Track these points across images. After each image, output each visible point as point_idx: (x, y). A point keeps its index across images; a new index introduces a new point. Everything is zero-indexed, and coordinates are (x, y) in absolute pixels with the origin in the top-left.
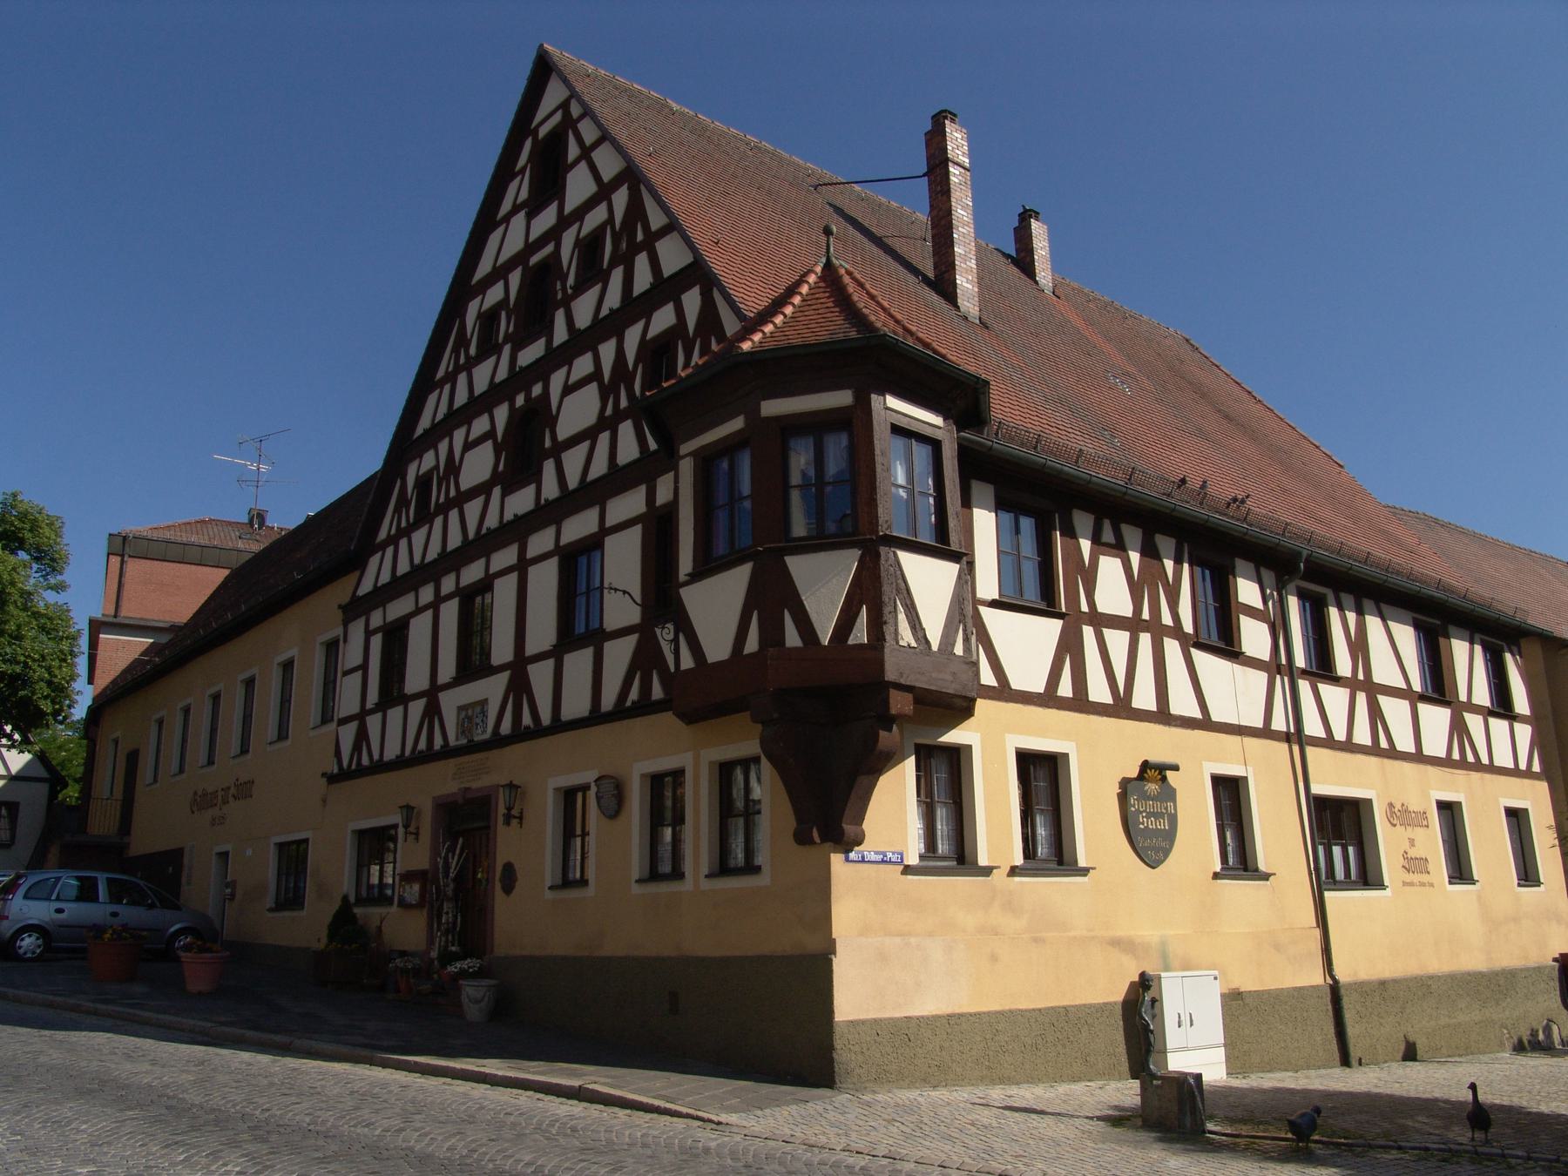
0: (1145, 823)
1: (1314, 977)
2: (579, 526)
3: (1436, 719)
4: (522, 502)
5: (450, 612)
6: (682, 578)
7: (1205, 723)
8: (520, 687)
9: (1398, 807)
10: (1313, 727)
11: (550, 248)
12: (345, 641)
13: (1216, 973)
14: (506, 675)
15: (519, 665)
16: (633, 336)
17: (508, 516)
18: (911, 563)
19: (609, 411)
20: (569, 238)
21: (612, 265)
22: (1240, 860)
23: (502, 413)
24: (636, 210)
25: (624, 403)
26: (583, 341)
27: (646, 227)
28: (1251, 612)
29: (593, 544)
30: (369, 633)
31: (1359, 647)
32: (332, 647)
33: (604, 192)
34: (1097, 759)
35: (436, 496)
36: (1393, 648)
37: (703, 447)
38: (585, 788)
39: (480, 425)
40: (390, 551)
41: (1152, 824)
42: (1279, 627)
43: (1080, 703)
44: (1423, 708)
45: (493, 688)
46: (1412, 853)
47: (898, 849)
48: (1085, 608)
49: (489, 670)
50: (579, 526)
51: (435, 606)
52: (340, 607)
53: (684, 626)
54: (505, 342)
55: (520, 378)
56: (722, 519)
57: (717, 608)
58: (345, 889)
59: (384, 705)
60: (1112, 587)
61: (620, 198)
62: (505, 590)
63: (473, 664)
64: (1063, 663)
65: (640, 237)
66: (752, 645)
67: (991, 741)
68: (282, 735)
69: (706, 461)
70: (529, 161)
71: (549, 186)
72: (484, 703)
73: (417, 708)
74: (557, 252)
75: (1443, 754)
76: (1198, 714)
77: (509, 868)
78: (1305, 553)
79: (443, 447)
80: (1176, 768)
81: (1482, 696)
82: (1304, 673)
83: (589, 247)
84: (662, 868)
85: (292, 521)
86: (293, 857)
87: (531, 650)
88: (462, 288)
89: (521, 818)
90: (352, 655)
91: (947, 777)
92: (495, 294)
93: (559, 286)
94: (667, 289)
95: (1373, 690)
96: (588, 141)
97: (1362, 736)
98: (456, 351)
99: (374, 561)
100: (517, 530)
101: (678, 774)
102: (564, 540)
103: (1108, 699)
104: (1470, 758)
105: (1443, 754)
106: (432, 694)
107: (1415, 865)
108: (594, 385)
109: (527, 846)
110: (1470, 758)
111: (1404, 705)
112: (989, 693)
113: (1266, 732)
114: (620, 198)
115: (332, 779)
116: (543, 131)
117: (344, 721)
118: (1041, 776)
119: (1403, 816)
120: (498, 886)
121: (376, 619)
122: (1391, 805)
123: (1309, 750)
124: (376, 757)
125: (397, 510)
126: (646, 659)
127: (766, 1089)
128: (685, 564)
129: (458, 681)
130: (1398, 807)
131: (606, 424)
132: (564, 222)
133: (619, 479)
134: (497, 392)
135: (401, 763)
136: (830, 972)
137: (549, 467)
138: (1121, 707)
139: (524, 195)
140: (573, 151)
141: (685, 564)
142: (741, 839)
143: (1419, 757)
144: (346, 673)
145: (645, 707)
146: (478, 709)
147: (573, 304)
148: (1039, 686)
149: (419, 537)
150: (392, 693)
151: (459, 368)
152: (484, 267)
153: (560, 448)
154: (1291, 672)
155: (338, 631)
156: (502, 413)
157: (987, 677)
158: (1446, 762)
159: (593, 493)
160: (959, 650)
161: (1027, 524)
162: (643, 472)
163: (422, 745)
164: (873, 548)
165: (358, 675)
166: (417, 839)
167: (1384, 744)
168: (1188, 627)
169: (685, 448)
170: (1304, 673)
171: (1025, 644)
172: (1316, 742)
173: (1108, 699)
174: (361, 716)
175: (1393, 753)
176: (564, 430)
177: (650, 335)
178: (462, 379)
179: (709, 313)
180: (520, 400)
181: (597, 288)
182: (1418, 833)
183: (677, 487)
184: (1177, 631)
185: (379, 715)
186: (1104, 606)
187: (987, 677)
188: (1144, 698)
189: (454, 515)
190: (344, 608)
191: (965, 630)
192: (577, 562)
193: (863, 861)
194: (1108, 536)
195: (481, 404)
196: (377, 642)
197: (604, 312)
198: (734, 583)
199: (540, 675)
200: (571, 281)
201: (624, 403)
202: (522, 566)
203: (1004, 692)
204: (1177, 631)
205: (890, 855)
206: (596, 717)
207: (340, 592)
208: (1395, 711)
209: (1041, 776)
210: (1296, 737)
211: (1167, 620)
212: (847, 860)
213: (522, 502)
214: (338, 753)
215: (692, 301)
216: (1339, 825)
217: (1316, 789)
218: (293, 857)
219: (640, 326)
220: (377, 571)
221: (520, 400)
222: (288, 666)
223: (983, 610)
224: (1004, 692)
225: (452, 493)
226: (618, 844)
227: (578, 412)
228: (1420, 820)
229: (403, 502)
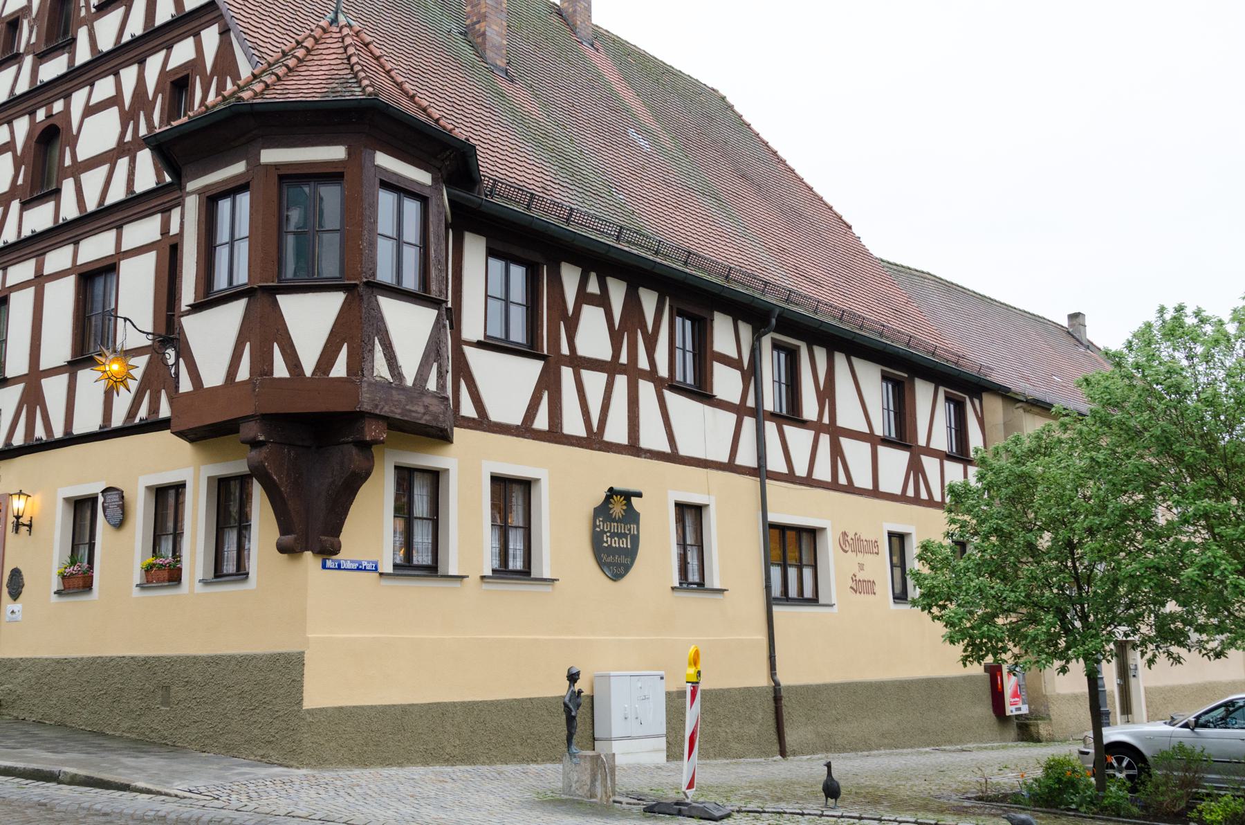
0: (608, 541)
1: (763, 681)
2: (96, 248)
3: (894, 462)
4: (40, 218)
6: (184, 308)
7: (673, 457)
8: (33, 399)
9: (851, 535)
10: (776, 462)
13: (662, 673)
14: (21, 386)
15: (34, 378)
16: (154, 65)
17: (26, 233)
18: (390, 308)
19: (128, 138)
22: (692, 579)
25: (143, 131)
26: (105, 63)
28: (726, 360)
29: (107, 269)
31: (827, 395)
34: (567, 489)
36: (861, 396)
38: (93, 500)
41: (615, 543)
42: (751, 374)
43: (555, 435)
44: (883, 451)
46: (860, 576)
48: (565, 350)
50: (96, 248)
54: (27, 53)
55: (41, 93)
56: (222, 255)
57: (214, 338)
60: (593, 335)
66: (243, 374)
67: (468, 464)
69: (211, 200)
75: (898, 491)
76: (667, 449)
77: (16, 573)
78: (777, 311)
80: (639, 495)
81: (942, 440)
82: (774, 416)
84: (164, 574)
89: (30, 526)
91: (420, 496)
95: (836, 433)
97: (823, 471)
102: (81, 260)
103: (581, 432)
104: (924, 495)
105: (898, 491)
107: (862, 586)
108: (115, 110)
110: (924, 495)
111: (866, 447)
112: (467, 423)
113: (730, 467)
118: (511, 494)
119: (850, 543)
120: (5, 590)
122: (845, 534)
123: (770, 484)
126: (157, 379)
128: (188, 296)
130: (851, 535)
131: (124, 149)
133: (136, 206)
137: (68, 186)
138: (594, 440)
141: (188, 296)
142: (234, 547)
143: (875, 493)
145: (154, 425)
147: (96, 24)
148: (517, 419)
153: (80, 168)
154: (758, 413)
156: (22, 126)
157: (467, 409)
158: (902, 498)
160: (432, 385)
162: (158, 201)
164: (361, 294)
167: (842, 480)
168: (663, 371)
169: (191, 186)
170: (774, 416)
171: (506, 384)
172: (777, 476)
173: (581, 432)
175: (850, 489)
176: (84, 151)
179: (225, 50)
180: (41, 115)
181: (120, 12)
182: (868, 559)
184: (652, 375)
186: (582, 351)
187: (467, 409)
188: (616, 431)
191: (439, 367)
192: (94, 280)
193: (339, 568)
194: (593, 287)
198: (231, 315)
199: (55, 389)
202: (40, 280)
204: (652, 375)
205: (364, 564)
208: (858, 454)
209: (511, 494)
210: (760, 472)
211: (643, 363)
212: (324, 567)
213: (40, 218)
215: (210, 37)
216: (791, 546)
217: (773, 517)
221: (41, 115)
224: (483, 423)
226: (122, 551)
227: (98, 134)
228: (871, 548)
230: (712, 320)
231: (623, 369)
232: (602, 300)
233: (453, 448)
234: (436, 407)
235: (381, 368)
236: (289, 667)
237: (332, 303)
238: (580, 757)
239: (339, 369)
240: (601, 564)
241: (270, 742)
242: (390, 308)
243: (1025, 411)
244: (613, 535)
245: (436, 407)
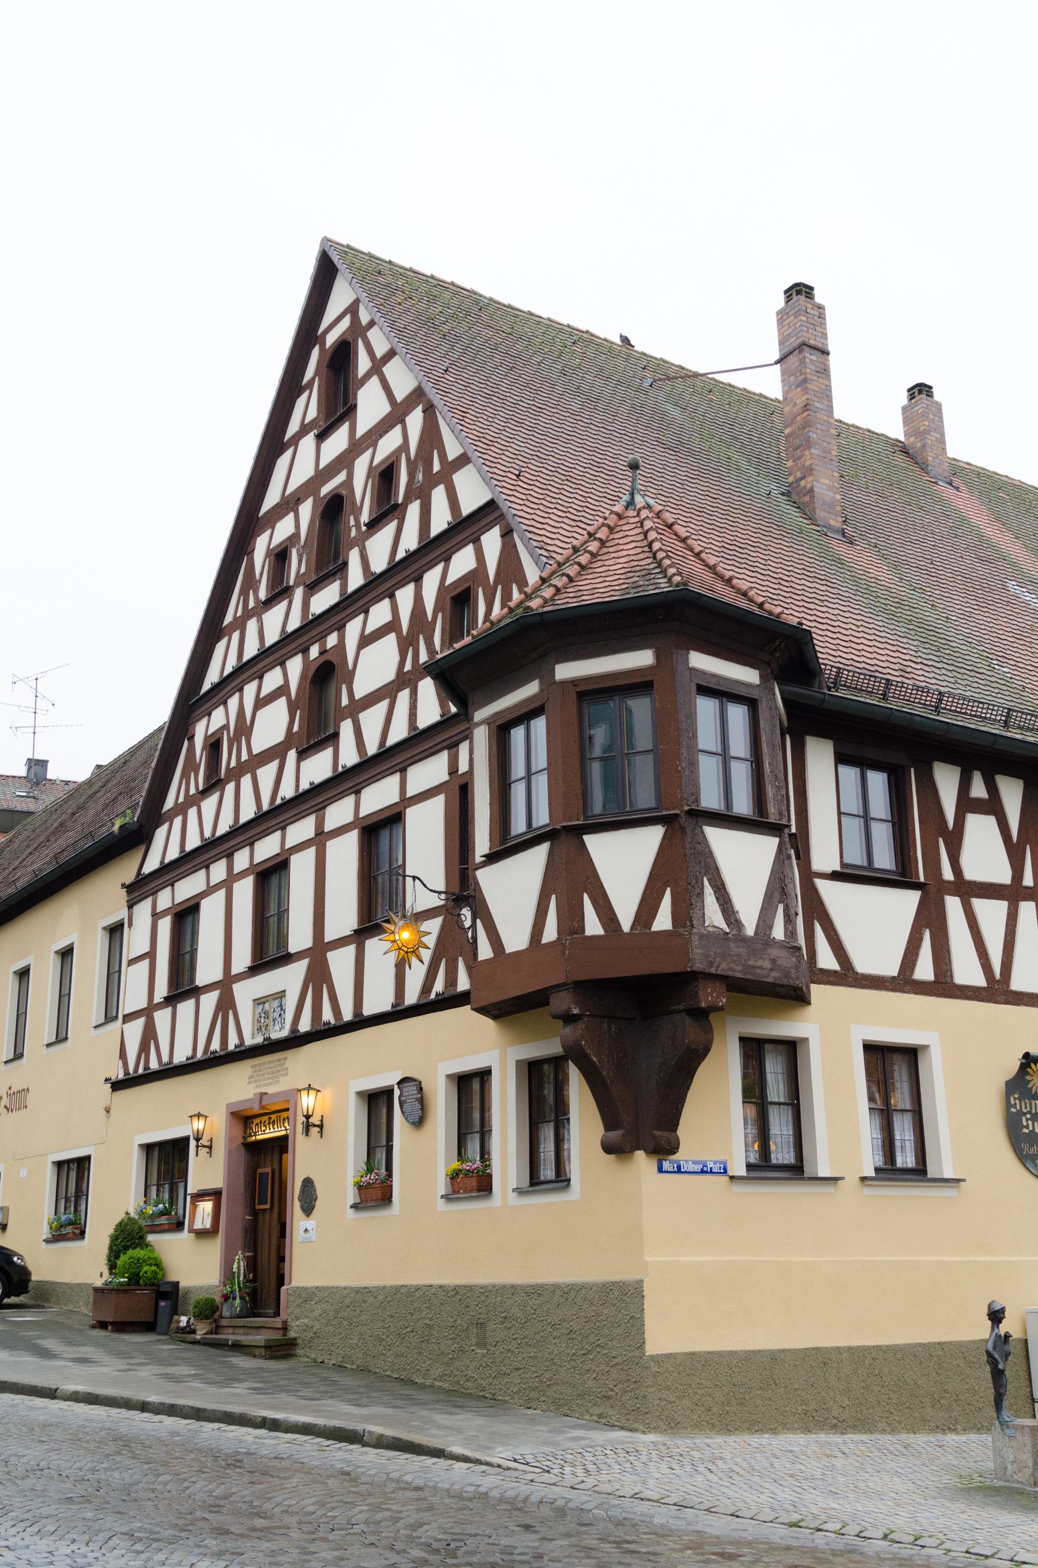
2: (379, 796)
5: (245, 890)
6: (478, 859)
8: (319, 977)
11: (342, 477)
12: (130, 925)
15: (319, 952)
16: (431, 580)
17: (304, 786)
19: (408, 667)
20: (361, 465)
21: (408, 499)
23: (295, 666)
24: (431, 436)
25: (423, 657)
26: (380, 586)
27: (443, 456)
29: (392, 819)
30: (156, 916)
32: (115, 931)
33: (397, 416)
35: (227, 759)
37: (497, 714)
38: (388, 1092)
39: (273, 680)
40: (178, 821)
43: (942, 985)
45: (290, 978)
47: (721, 1158)
48: (948, 874)
49: (286, 959)
50: (379, 796)
51: (228, 884)
52: (123, 886)
53: (481, 911)
55: (314, 627)
56: (518, 793)
57: (514, 892)
58: (310, 1223)
59: (172, 1000)
60: (984, 852)
61: (415, 420)
62: (302, 867)
63: (269, 954)
64: (920, 940)
65: (436, 467)
66: (550, 933)
67: (833, 1031)
68: (61, 1038)
70: (316, 373)
71: (339, 408)
72: (281, 995)
73: (209, 1001)
74: (349, 482)
77: (308, 1184)
79: (233, 702)
83: (386, 476)
84: (473, 1182)
85: (81, 773)
86: (74, 1173)
87: (330, 934)
88: (249, 522)
90: (136, 941)
91: (775, 1076)
92: (284, 528)
93: (352, 522)
94: (466, 528)
96: (380, 352)
98: (245, 593)
99: (161, 833)
100: (313, 799)
101: (484, 1074)
103: (981, 982)
106: (225, 985)
109: (326, 1162)
114: (415, 420)
115: (117, 1086)
116: (331, 339)
117: (128, 1018)
118: (891, 1065)
120: (297, 1204)
121: (164, 900)
124: (165, 1059)
125: (185, 775)
126: (453, 945)
128: (482, 845)
129: (255, 969)
131: (405, 680)
132: (356, 447)
133: (420, 744)
134: (290, 643)
135: (191, 1067)
137: (346, 728)
138: (997, 990)
139: (312, 413)
140: (363, 364)
141: (482, 845)
142: (551, 1147)
144: (131, 962)
146: (276, 1003)
148: (892, 969)
149: (209, 805)
150: (183, 987)
151: (248, 614)
152: (272, 498)
155: (123, 914)
156: (295, 666)
157: (826, 960)
159: (392, 759)
160: (778, 932)
161: (878, 781)
163: (216, 1045)
164: (683, 825)
165: (145, 964)
166: (210, 1153)
169: (479, 715)
171: (874, 924)
173: (981, 982)
174: (148, 1012)
176: (362, 687)
177: (449, 581)
178: (252, 625)
180: (314, 651)
183: (476, 754)
185: (169, 1010)
186: (972, 872)
187: (826, 960)
189: (246, 781)
190: (130, 888)
191: (786, 909)
192: (379, 832)
193: (679, 1171)
194: (978, 790)
195: (272, 656)
196: (165, 925)
197: (401, 555)
198: (531, 866)
199: (341, 963)
200: (365, 517)
201: (423, 657)
202: (321, 838)
203: (846, 975)
206: (398, 1013)
207: (126, 870)
209: (891, 1065)
213: (318, 768)
214: (123, 1055)
215: (492, 541)
218: (74, 1173)
219: (439, 569)
220: (165, 845)
221: (314, 651)
222: (66, 954)
223: (821, 884)
224: (846, 975)
225: (245, 757)
227: (375, 666)
229: (191, 766)
232: (993, 806)
234: (786, 960)
235: (713, 916)
239: (663, 921)
241: (608, 1398)
242: (721, 841)
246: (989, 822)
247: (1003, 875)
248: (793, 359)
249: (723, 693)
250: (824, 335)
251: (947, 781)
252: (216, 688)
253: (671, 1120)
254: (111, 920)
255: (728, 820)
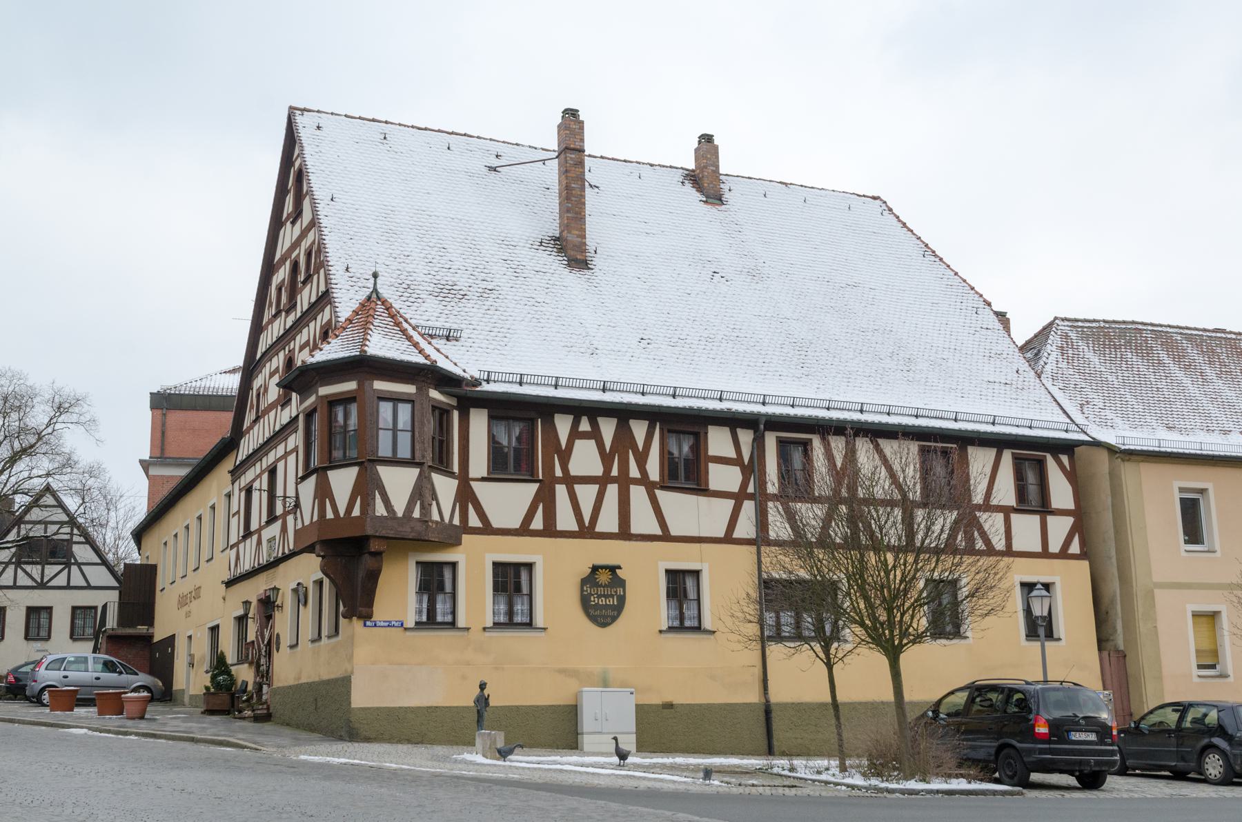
0: (594, 600)
18: (385, 472)
30: (240, 490)
34: (557, 569)
43: (550, 530)
48: (558, 472)
67: (474, 562)
76: (659, 532)
78: (763, 420)
80: (620, 568)
82: (775, 498)
91: (435, 581)
103: (574, 527)
104: (980, 545)
127: (304, 735)
136: (691, 707)
138: (587, 531)
164: (368, 464)
173: (574, 527)
184: (644, 480)
186: (575, 469)
187: (474, 521)
190: (232, 472)
194: (585, 426)
196: (243, 494)
203: (487, 529)
204: (644, 480)
207: (228, 464)
211: (634, 472)
220: (247, 446)
224: (487, 529)
230: (706, 433)
231: (614, 480)
232: (595, 434)
233: (460, 548)
234: (419, 527)
235: (380, 510)
236: (343, 685)
237: (353, 472)
238: (456, 761)
239: (356, 512)
240: (593, 619)
242: (385, 472)
243: (1123, 460)
244: (599, 597)
245: (419, 527)
246: (591, 444)
247: (598, 470)
248: (562, 156)
249: (395, 399)
250: (582, 140)
251: (563, 425)
252: (264, 355)
253: (370, 604)
254: (226, 491)
255: (394, 462)
